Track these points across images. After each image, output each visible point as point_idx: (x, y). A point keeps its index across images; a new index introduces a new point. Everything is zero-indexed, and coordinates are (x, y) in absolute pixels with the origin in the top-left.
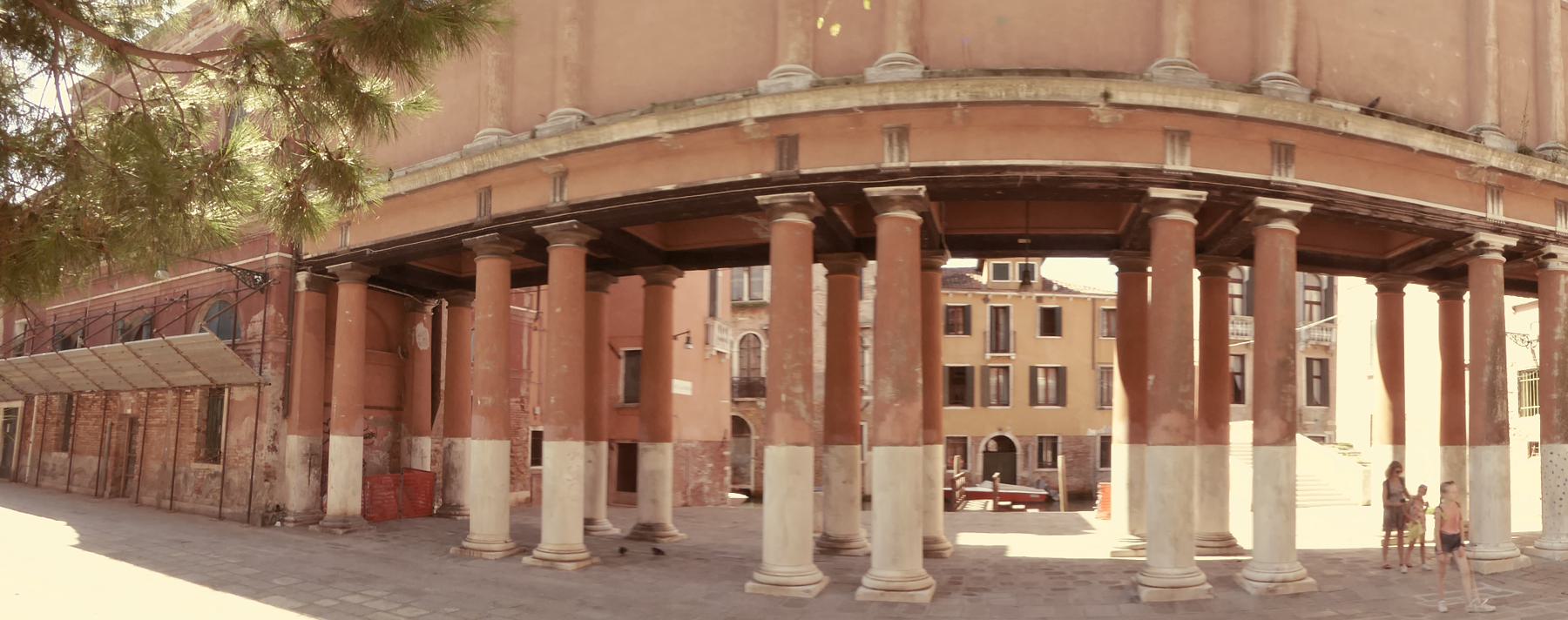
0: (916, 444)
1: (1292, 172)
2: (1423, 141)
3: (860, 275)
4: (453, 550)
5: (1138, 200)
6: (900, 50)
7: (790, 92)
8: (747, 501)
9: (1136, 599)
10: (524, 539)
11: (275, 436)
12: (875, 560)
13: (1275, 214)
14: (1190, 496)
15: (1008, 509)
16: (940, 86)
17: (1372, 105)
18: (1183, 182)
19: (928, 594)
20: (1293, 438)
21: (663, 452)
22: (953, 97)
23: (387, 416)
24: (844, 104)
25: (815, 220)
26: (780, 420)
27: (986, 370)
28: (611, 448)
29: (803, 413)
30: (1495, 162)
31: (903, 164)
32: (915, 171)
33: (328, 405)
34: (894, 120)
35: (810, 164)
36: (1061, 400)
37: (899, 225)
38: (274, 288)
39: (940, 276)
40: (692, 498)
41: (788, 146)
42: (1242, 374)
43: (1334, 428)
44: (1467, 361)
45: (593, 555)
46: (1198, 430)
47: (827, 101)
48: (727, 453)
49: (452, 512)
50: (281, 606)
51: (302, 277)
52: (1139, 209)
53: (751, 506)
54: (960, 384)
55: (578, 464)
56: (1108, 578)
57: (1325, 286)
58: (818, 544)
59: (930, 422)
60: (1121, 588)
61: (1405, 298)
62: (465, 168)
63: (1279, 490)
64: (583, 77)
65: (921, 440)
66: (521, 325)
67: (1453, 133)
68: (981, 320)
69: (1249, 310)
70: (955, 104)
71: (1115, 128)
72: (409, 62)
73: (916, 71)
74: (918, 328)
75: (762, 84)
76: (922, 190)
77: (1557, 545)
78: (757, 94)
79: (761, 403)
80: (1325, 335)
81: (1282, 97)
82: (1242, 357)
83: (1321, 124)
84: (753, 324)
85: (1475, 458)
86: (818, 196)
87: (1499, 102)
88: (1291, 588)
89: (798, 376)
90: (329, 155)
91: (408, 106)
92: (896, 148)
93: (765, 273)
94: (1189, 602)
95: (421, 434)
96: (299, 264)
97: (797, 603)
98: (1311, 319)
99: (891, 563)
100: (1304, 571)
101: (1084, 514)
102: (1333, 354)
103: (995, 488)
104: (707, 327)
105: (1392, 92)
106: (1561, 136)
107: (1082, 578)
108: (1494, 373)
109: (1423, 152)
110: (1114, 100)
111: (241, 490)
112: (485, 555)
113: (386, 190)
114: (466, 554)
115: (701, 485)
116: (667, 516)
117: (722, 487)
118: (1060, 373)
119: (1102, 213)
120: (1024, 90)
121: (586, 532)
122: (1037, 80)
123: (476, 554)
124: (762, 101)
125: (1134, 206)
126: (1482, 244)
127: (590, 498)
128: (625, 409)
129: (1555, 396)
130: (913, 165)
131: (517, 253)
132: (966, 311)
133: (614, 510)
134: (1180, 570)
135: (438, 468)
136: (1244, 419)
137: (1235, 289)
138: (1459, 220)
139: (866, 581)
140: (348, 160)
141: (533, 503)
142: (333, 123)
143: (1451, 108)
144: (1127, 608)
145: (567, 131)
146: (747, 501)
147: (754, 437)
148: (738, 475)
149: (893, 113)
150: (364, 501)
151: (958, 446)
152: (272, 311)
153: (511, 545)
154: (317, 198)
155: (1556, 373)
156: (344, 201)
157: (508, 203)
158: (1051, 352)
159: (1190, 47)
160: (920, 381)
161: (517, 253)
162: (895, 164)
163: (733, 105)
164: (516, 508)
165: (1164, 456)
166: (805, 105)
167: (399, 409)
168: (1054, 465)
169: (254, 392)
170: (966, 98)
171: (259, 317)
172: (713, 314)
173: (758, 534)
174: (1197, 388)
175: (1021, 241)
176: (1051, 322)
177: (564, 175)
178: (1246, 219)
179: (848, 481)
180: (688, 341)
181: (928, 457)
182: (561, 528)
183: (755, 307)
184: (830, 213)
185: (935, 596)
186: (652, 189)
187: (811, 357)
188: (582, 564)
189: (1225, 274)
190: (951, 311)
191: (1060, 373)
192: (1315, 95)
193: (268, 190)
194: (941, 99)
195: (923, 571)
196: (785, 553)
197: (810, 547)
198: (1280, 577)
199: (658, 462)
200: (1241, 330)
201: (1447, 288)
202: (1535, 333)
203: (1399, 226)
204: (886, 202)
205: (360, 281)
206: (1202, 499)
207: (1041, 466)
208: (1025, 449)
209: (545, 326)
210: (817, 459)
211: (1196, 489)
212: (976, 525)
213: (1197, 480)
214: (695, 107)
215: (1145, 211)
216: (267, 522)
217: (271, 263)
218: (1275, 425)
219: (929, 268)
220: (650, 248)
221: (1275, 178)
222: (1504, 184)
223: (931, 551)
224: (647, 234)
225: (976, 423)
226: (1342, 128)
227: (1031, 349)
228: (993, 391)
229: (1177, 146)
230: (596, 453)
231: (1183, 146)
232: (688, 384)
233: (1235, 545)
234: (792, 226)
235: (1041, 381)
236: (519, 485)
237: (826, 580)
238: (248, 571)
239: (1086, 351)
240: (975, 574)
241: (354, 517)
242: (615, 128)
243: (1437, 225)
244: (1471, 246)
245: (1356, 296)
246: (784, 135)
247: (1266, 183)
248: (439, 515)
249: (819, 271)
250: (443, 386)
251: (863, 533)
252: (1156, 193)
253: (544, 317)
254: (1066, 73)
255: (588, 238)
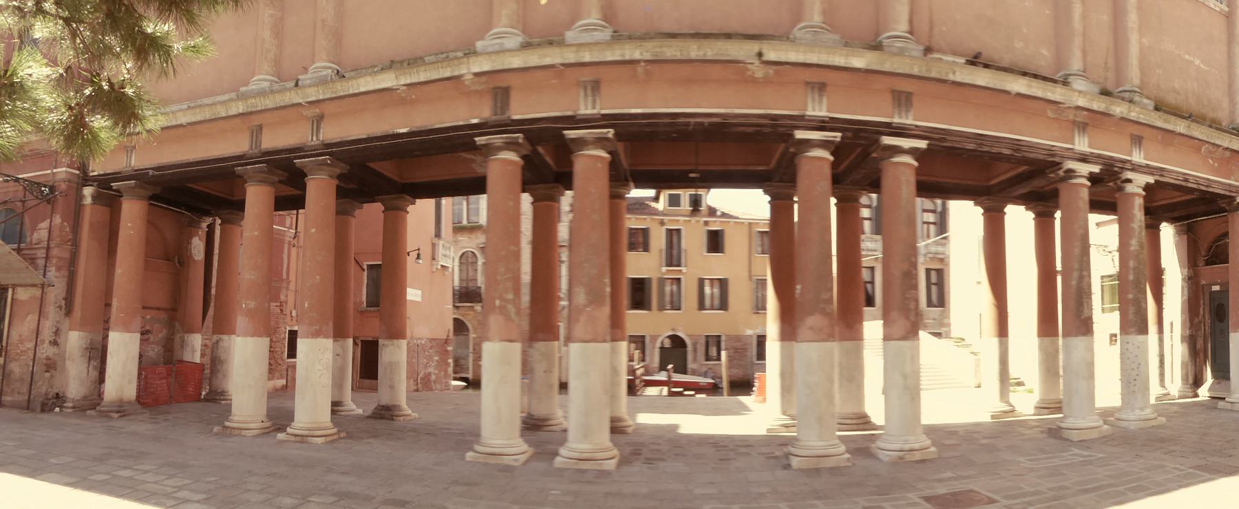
0: (605, 341)
1: (911, 115)
2: (1019, 85)
3: (558, 202)
4: (216, 429)
5: (785, 141)
6: (594, 18)
7: (502, 51)
8: (466, 387)
9: (788, 466)
10: (279, 418)
11: (57, 332)
12: (571, 435)
13: (897, 150)
14: (831, 381)
15: (680, 394)
16: (627, 46)
17: (976, 57)
18: (822, 125)
19: (614, 462)
20: (917, 334)
21: (399, 347)
22: (637, 55)
23: (163, 316)
24: (548, 61)
25: (524, 157)
26: (495, 321)
27: (662, 281)
28: (355, 343)
29: (513, 316)
30: (1081, 102)
31: (595, 111)
32: (605, 117)
33: (108, 305)
34: (587, 75)
35: (518, 112)
36: (724, 305)
37: (591, 162)
38: (60, 199)
39: (625, 204)
40: (422, 384)
41: (502, 95)
42: (872, 282)
43: (949, 325)
44: (1059, 267)
45: (339, 432)
46: (837, 329)
47: (534, 58)
48: (450, 348)
49: (217, 397)
50: (56, 483)
51: (88, 191)
52: (787, 148)
53: (470, 391)
54: (640, 293)
55: (328, 357)
56: (764, 450)
57: (939, 209)
58: (524, 422)
59: (616, 323)
60: (776, 457)
61: (1006, 217)
62: (239, 108)
63: (905, 377)
64: (337, 37)
65: (608, 338)
66: (282, 242)
67: (1045, 79)
68: (658, 240)
69: (877, 230)
70: (638, 62)
71: (766, 81)
72: (188, 11)
73: (606, 34)
74: (607, 246)
75: (479, 45)
76: (610, 133)
77: (1132, 417)
78: (475, 53)
79: (478, 307)
80: (940, 249)
81: (901, 53)
82: (872, 269)
83: (933, 75)
84: (471, 243)
85: (1066, 346)
86: (527, 138)
87: (1084, 53)
88: (918, 456)
89: (509, 285)
90: (111, 85)
91: (186, 49)
92: (590, 99)
93: (483, 200)
94: (832, 468)
95: (191, 331)
96: (85, 180)
97: (508, 469)
98: (928, 237)
99: (584, 437)
100: (929, 442)
101: (743, 399)
102: (947, 265)
103: (669, 377)
104: (434, 245)
105: (992, 46)
106: (1137, 81)
107: (743, 450)
108: (1081, 278)
109: (1019, 95)
110: (765, 58)
111: (22, 380)
112: (244, 432)
113: (162, 121)
114: (228, 432)
115: (430, 374)
116: (402, 399)
117: (446, 376)
118: (723, 284)
119: (757, 152)
120: (694, 50)
121: (333, 412)
122: (706, 42)
123: (236, 432)
124: (480, 58)
125: (783, 146)
126: (1070, 171)
127: (338, 384)
128: (367, 312)
129: (1130, 296)
130: (604, 112)
131: (280, 182)
132: (645, 232)
133: (358, 394)
134: (823, 443)
135: (207, 360)
136: (875, 319)
137: (865, 213)
138: (1051, 151)
139: (563, 451)
140: (129, 91)
141: (288, 389)
142: (118, 56)
143: (1043, 58)
144: (781, 473)
145: (323, 82)
146: (466, 387)
147: (472, 335)
148: (459, 366)
149: (587, 70)
150: (139, 386)
151: (639, 342)
152: (57, 220)
153: (268, 424)
154: (99, 122)
155: (1131, 277)
156: (124, 127)
157: (274, 140)
158: (716, 266)
159: (824, 13)
160: (608, 290)
161: (280, 182)
162: (590, 111)
163: (456, 62)
164: (274, 394)
165: (809, 351)
166: (516, 62)
167: (174, 310)
168: (719, 359)
169: (38, 292)
170: (648, 56)
171: (45, 225)
172: (438, 235)
173: (478, 414)
174: (830, 296)
175: (692, 175)
176: (715, 242)
177: (320, 119)
178: (874, 155)
179: (548, 371)
180: (418, 257)
181: (614, 352)
182: (311, 409)
183: (473, 229)
184: (535, 151)
185: (620, 464)
186: (391, 132)
187: (519, 270)
188: (329, 439)
189: (857, 200)
190: (633, 232)
191: (723, 284)
192: (928, 50)
193: (50, 111)
194: (627, 58)
195: (609, 444)
196: (499, 431)
197: (518, 425)
198: (907, 447)
199: (394, 355)
200: (871, 247)
201: (1041, 208)
202: (1115, 243)
203: (999, 157)
204: (581, 143)
205: (141, 198)
206: (841, 386)
207: (707, 359)
208: (695, 345)
209: (301, 243)
210: (524, 353)
211: (836, 377)
212: (654, 407)
213: (837, 370)
214: (425, 63)
215: (792, 150)
216: (46, 407)
217: (59, 177)
218: (901, 325)
219: (616, 197)
220: (390, 180)
221: (896, 120)
222: (1089, 120)
223: (617, 428)
224: (386, 168)
225: (654, 324)
226: (951, 77)
227: (699, 264)
228: (668, 298)
229: (816, 96)
230: (344, 348)
231: (821, 96)
232: (419, 292)
233: (869, 422)
234: (505, 162)
235: (707, 290)
236: (277, 375)
237: (531, 451)
238: (24, 452)
239: (745, 265)
240: (653, 447)
241: (129, 402)
242: (362, 81)
243: (1031, 155)
244: (1061, 173)
245: (966, 216)
246: (499, 87)
247: (889, 125)
248: (207, 400)
249: (526, 199)
250: (213, 291)
251: (559, 413)
252: (800, 135)
253: (301, 235)
254: (728, 36)
255: (338, 171)
